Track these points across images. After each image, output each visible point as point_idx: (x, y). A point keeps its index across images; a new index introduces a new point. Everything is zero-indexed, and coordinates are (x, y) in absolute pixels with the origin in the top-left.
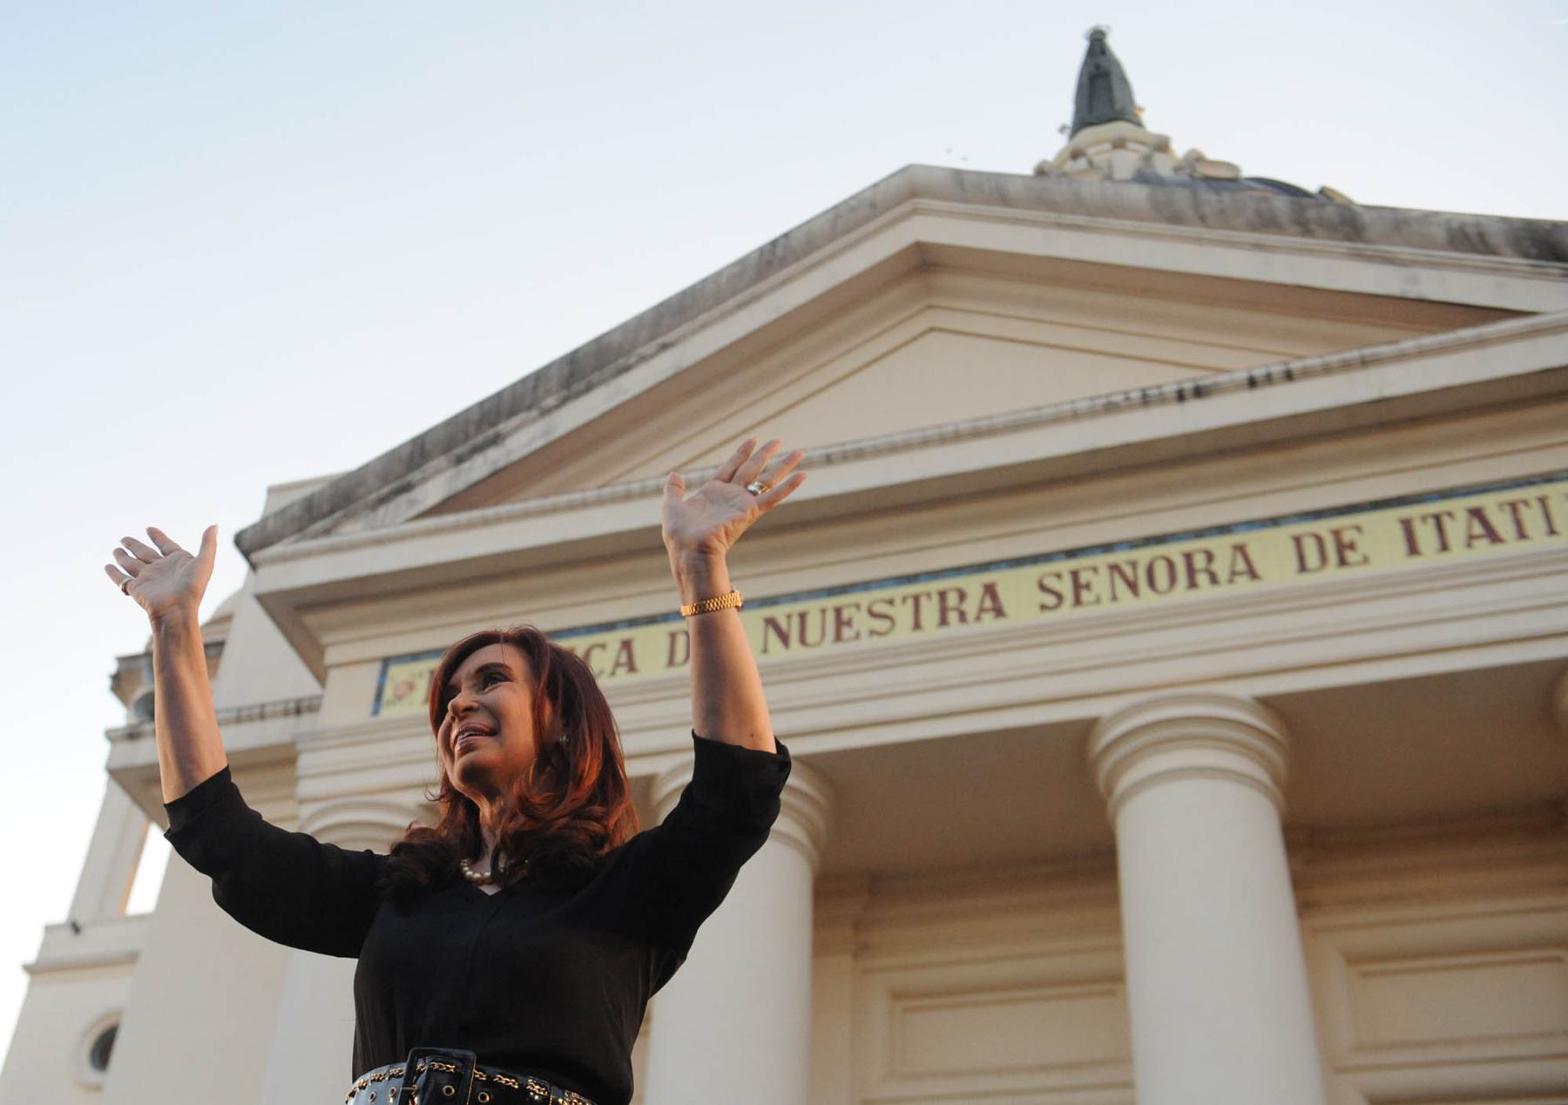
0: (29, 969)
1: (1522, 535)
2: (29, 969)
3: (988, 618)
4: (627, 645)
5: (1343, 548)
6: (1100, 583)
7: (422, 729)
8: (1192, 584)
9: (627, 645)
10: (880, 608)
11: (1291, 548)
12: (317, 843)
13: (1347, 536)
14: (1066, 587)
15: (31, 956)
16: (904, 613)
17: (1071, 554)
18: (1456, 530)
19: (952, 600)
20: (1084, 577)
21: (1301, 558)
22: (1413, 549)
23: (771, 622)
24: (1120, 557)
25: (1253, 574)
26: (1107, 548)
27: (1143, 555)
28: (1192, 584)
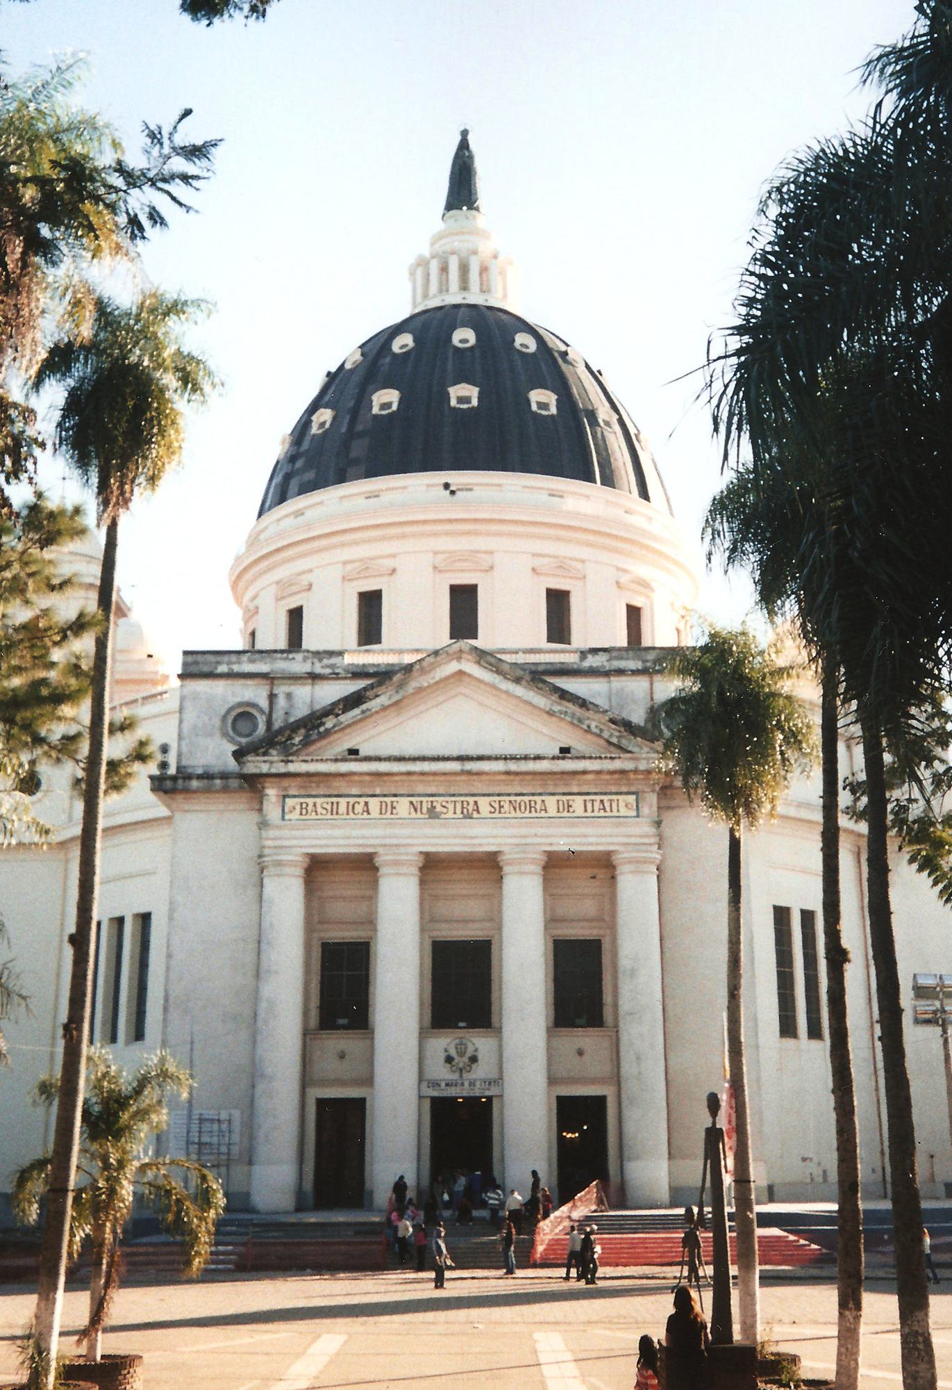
0: (179, 676)
1: (611, 811)
2: (179, 676)
3: (543, 812)
4: (366, 803)
5: (569, 806)
6: (507, 806)
7: (532, 868)
8: (530, 812)
9: (366, 803)
10: (444, 804)
11: (555, 802)
12: (837, 821)
13: (571, 803)
14: (497, 806)
15: (180, 672)
16: (451, 807)
17: (499, 795)
18: (597, 805)
19: (304, 805)
20: (395, 804)
21: (585, 807)
22: (586, 811)
23: (411, 803)
24: (512, 798)
25: (369, 813)
26: (509, 795)
27: (519, 799)
28: (530, 812)
